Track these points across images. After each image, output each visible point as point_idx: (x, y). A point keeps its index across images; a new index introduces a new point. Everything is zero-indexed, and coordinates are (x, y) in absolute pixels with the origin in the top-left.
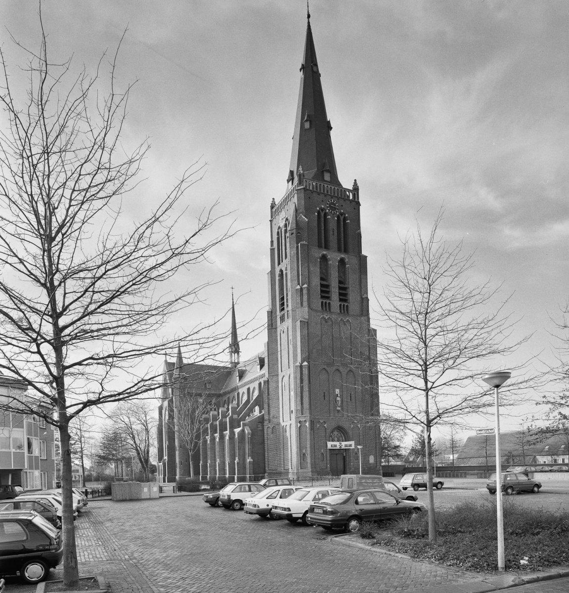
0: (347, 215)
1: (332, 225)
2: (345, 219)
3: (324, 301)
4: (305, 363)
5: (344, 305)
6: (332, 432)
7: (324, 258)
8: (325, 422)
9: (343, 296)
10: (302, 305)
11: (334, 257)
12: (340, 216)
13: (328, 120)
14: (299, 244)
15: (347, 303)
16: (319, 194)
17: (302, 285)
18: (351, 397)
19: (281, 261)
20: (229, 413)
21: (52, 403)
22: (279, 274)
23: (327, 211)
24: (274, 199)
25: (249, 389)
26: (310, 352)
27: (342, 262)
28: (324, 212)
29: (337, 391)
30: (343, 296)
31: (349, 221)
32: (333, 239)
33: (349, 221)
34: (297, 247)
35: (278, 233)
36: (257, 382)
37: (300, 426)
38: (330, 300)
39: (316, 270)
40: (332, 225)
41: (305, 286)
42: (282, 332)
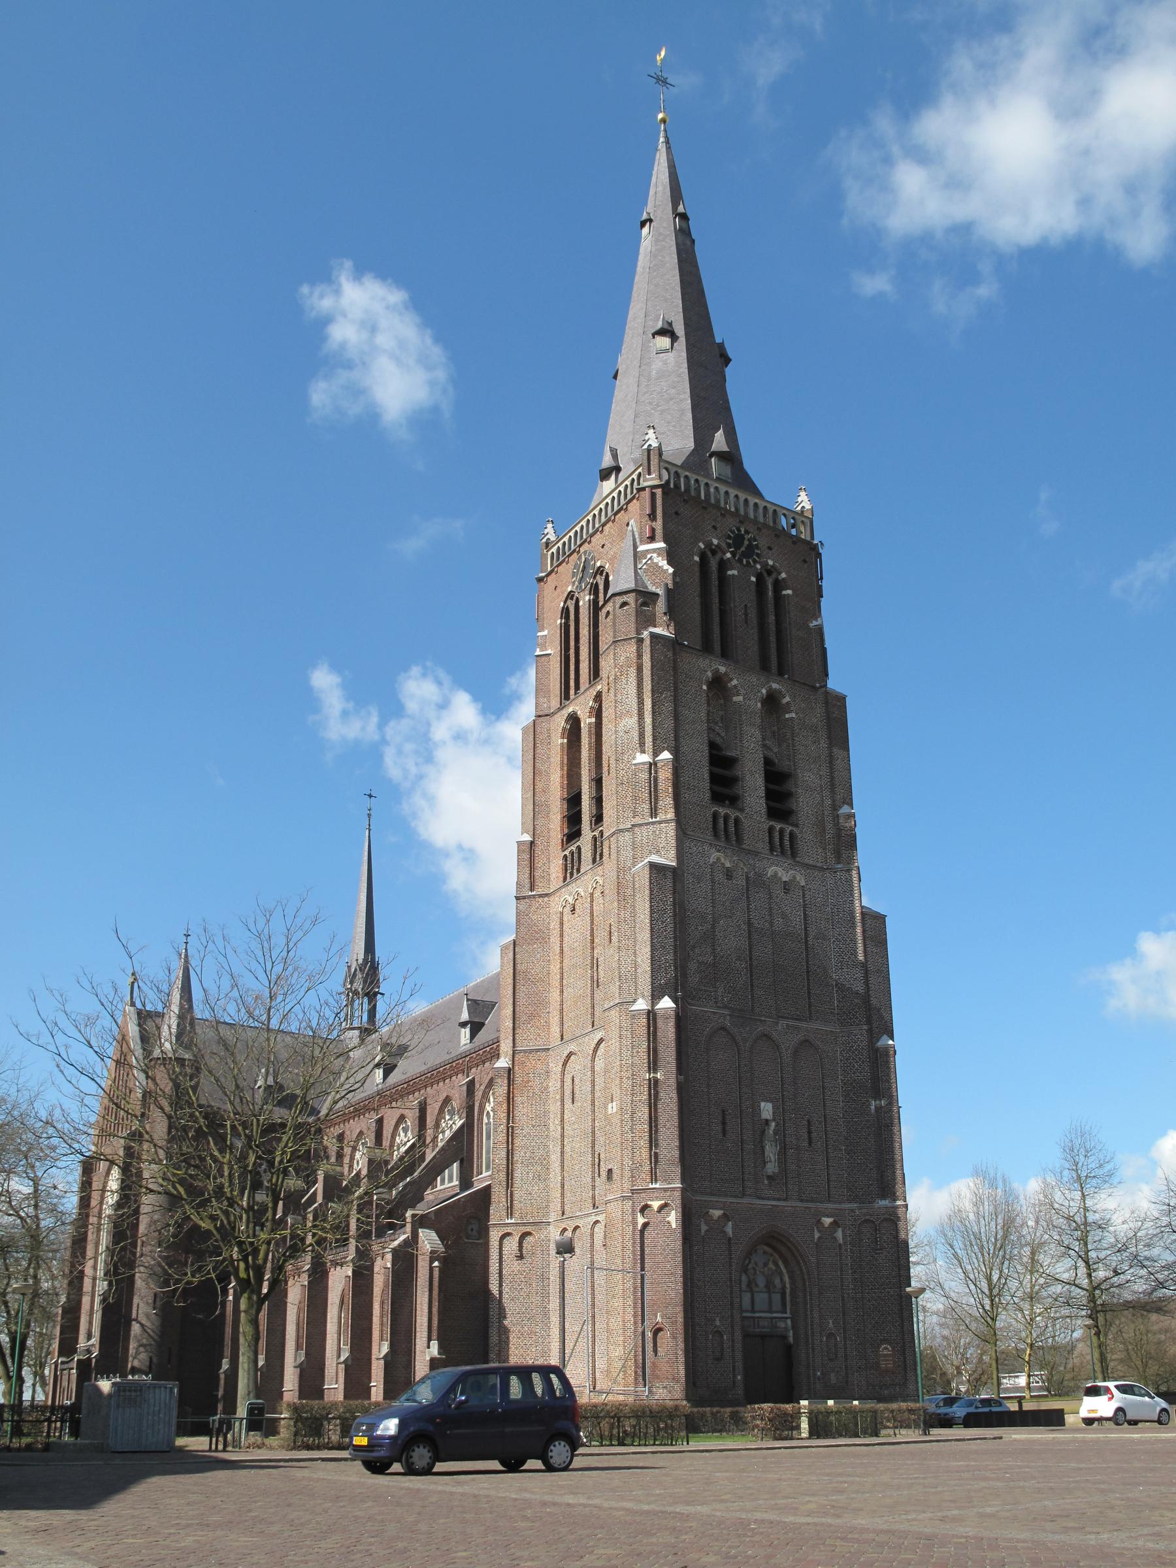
0: (783, 575)
1: (742, 600)
2: (778, 586)
3: (722, 811)
4: (666, 1003)
5: (781, 831)
6: (749, 1255)
7: (717, 683)
8: (644, 1208)
9: (779, 802)
10: (654, 812)
11: (748, 690)
12: (765, 575)
13: (718, 340)
14: (645, 634)
15: (792, 825)
16: (705, 508)
17: (656, 754)
18: (809, 1132)
19: (572, 692)
20: (315, 1193)
21: (1000, 1405)
22: (564, 729)
23: (729, 555)
24: (654, 335)
25: (471, 1085)
26: (681, 967)
27: (772, 702)
28: (718, 557)
29: (767, 1109)
30: (779, 802)
31: (789, 592)
32: (747, 639)
33: (789, 592)
34: (640, 641)
35: (565, 612)
36: (414, 1101)
37: (645, 1225)
38: (742, 810)
39: (698, 712)
40: (742, 600)
41: (666, 755)
42: (568, 910)
